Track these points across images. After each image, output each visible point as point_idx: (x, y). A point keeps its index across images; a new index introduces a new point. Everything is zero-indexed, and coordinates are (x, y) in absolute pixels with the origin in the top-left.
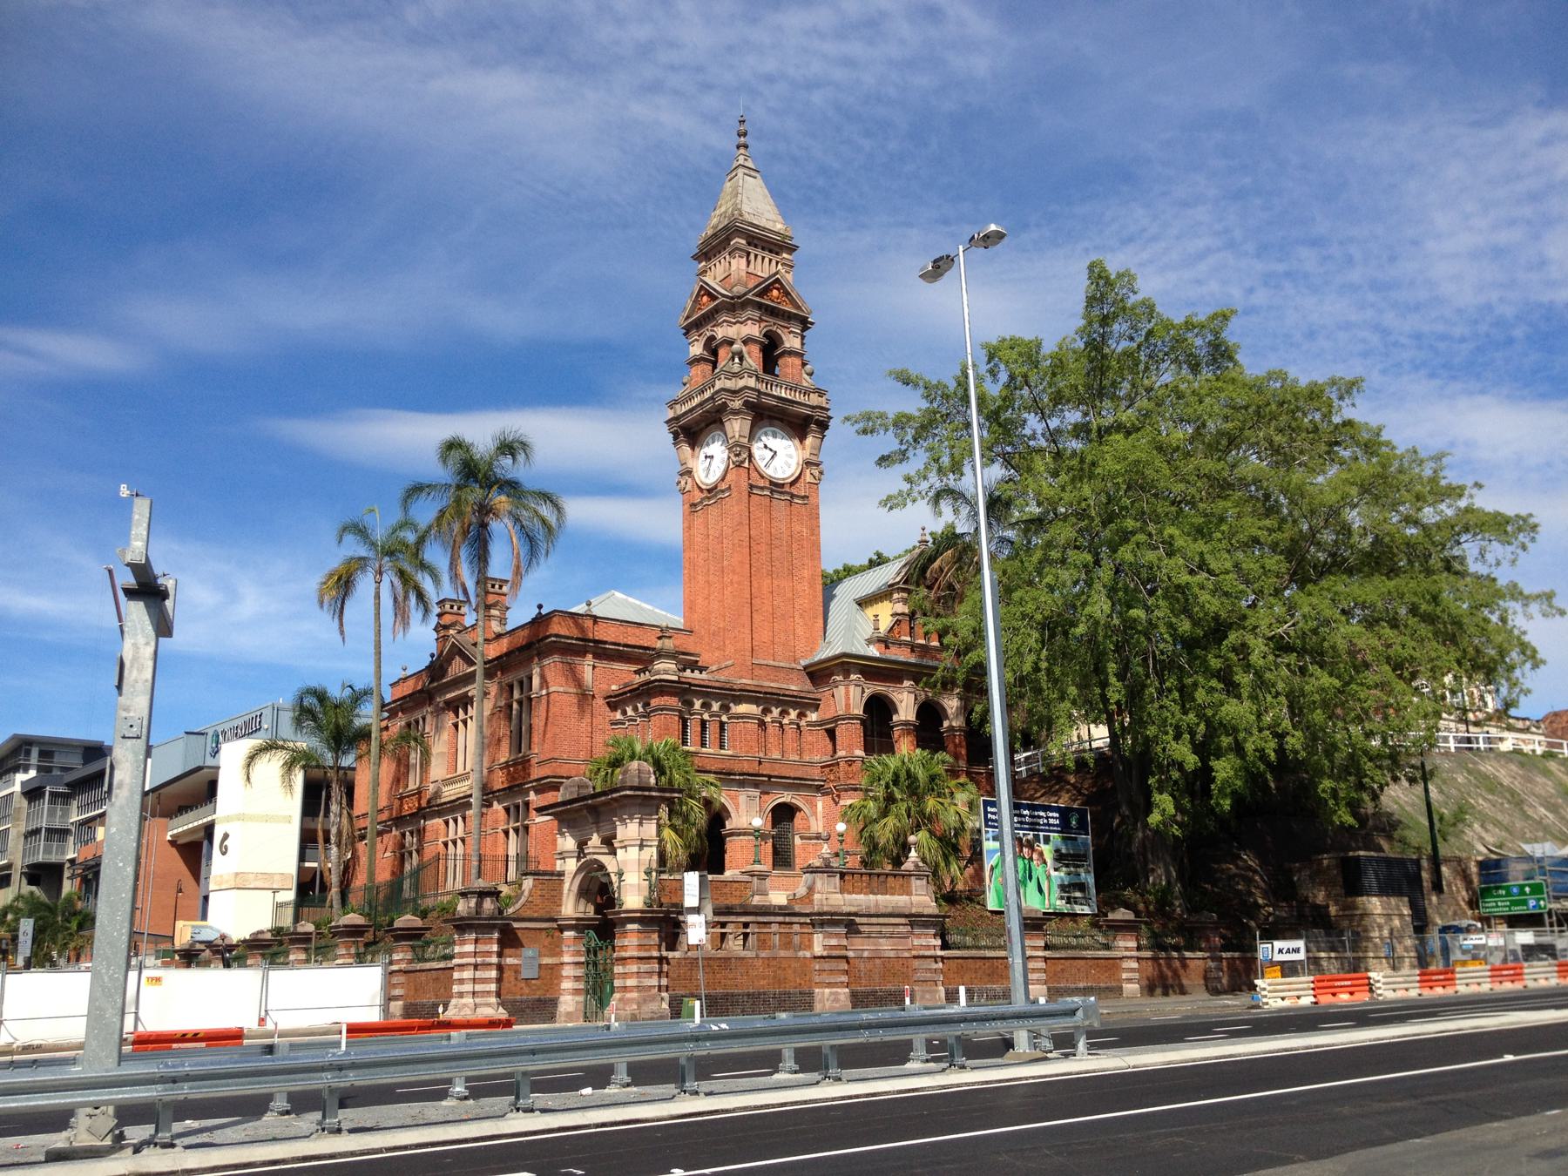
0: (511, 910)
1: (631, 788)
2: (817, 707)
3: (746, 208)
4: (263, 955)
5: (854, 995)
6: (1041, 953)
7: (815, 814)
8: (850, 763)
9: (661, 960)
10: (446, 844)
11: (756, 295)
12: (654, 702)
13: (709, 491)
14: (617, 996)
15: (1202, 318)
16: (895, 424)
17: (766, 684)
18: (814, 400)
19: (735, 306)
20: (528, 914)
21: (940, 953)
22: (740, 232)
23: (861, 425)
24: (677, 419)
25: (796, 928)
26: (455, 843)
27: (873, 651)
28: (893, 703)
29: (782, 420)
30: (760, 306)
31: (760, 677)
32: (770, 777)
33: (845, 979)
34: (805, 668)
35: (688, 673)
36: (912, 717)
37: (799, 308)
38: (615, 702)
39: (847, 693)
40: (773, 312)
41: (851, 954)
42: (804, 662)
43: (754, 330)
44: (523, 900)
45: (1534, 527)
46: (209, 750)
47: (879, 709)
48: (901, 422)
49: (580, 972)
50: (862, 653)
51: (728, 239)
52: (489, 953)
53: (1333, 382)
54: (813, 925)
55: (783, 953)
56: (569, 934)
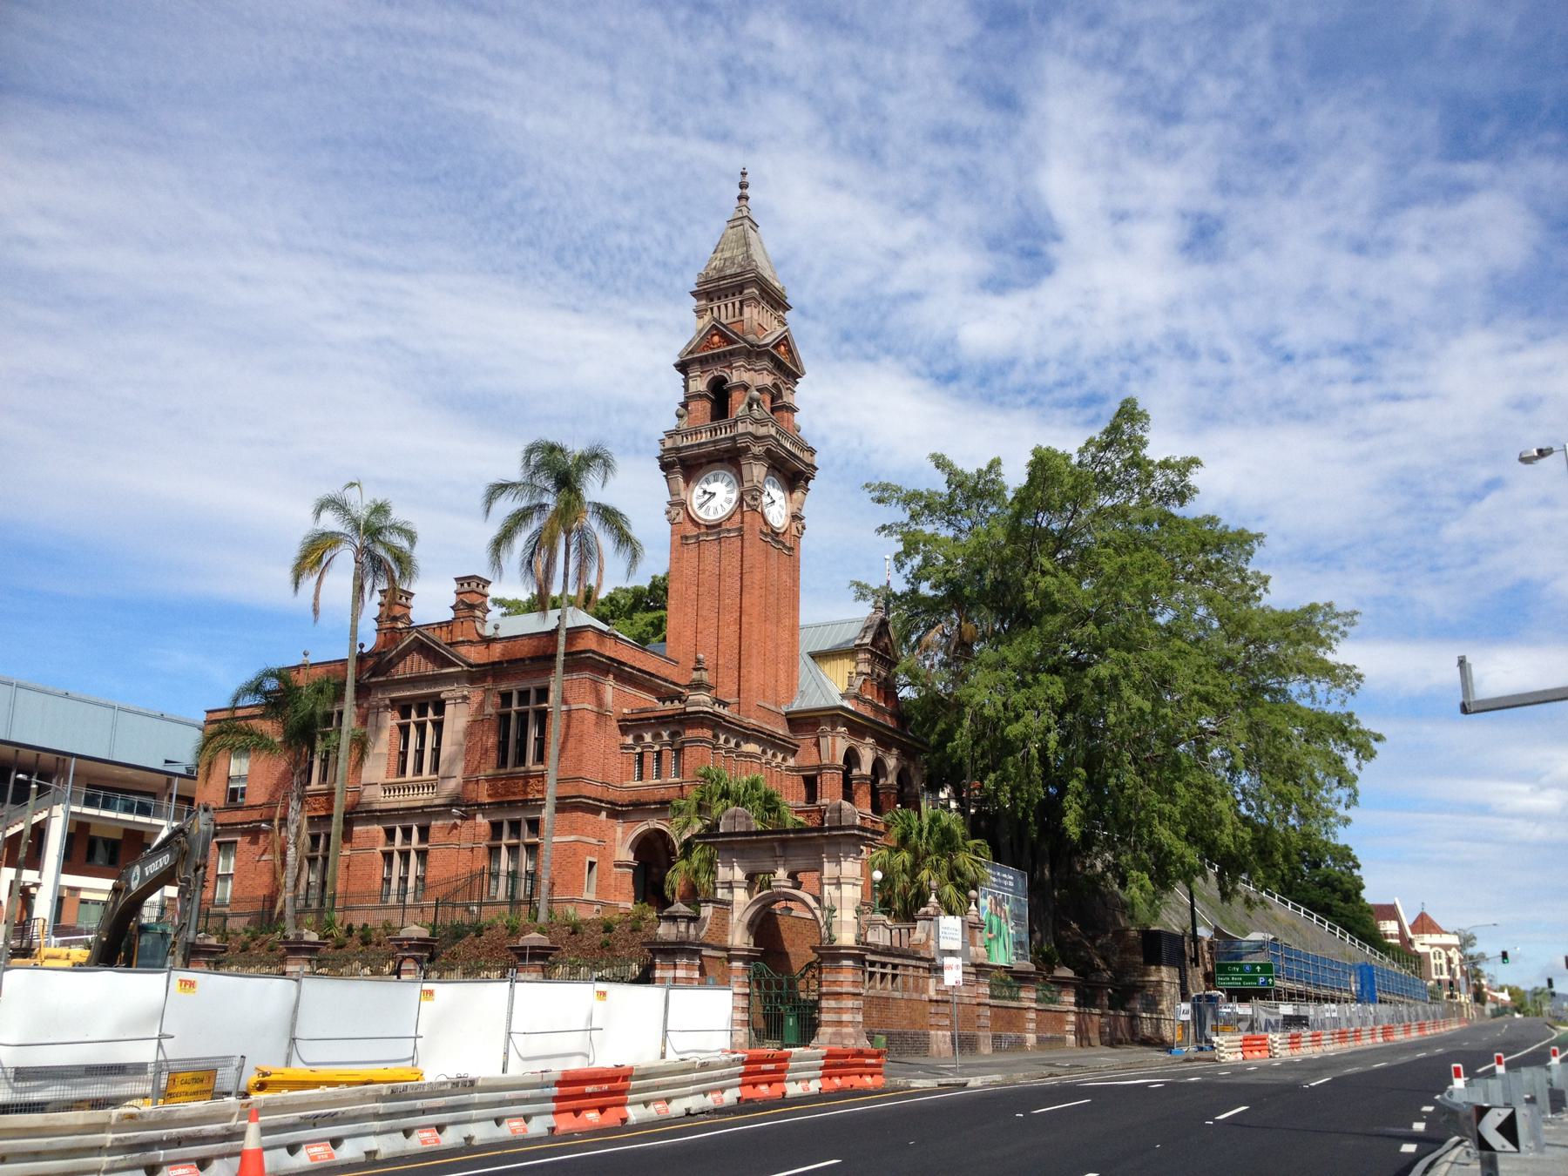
2: (794, 753)
4: (208, 963)
6: (1034, 1005)
10: (388, 856)
12: (690, 734)
19: (754, 353)
21: (988, 1001)
23: (877, 494)
26: (405, 855)
38: (629, 725)
39: (834, 744)
42: (784, 709)
43: (767, 380)
45: (1359, 677)
48: (911, 498)
51: (740, 288)
54: (929, 970)
56: (737, 965)
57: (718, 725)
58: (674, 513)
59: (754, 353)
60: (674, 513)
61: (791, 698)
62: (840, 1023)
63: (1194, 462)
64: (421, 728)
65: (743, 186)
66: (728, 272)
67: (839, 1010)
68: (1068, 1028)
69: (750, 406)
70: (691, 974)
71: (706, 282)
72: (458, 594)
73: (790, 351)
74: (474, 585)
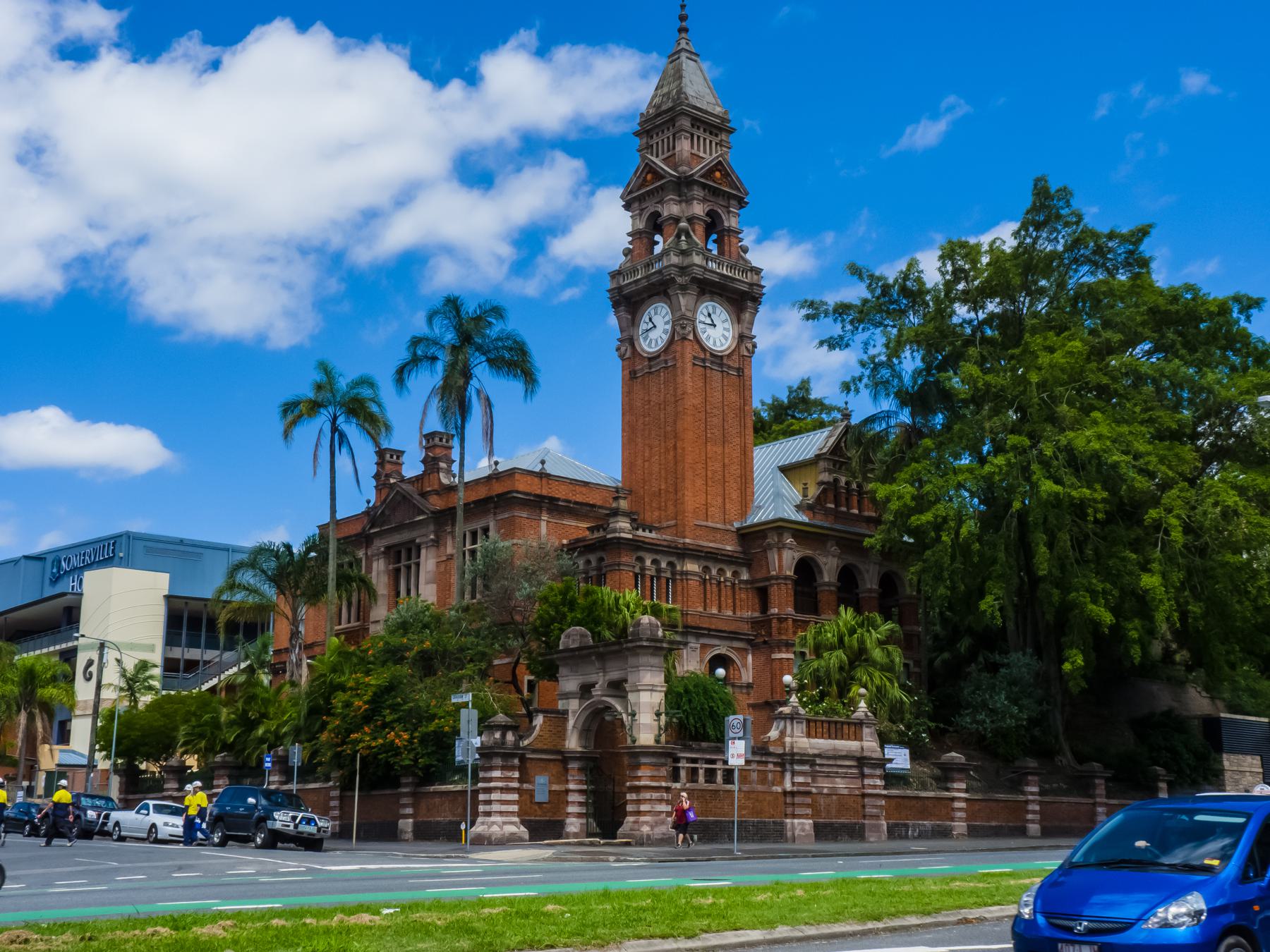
0: (526, 742)
1: (648, 640)
5: (816, 826)
6: (963, 795)
7: (745, 665)
8: (781, 620)
9: (668, 789)
11: (702, 176)
13: (650, 359)
14: (630, 819)
15: (1125, 230)
16: (835, 311)
17: (705, 544)
18: (750, 278)
19: (683, 185)
22: (684, 113)
24: (620, 289)
25: (771, 767)
27: (803, 518)
29: (721, 295)
30: (704, 186)
33: (809, 811)
34: (738, 529)
35: (640, 532)
36: (834, 579)
37: (738, 189)
40: (715, 192)
41: (814, 790)
42: (737, 525)
46: (48, 575)
48: (842, 310)
49: (581, 799)
50: (793, 518)
51: (672, 121)
53: (1237, 299)
55: (760, 788)
56: (573, 765)
58: (623, 349)
60: (623, 349)
61: (744, 514)
62: (639, 813)
65: (683, 18)
66: (664, 108)
67: (638, 802)
68: (1030, 816)
69: (678, 236)
70: (510, 774)
72: (427, 449)
73: (726, 175)
74: (437, 440)
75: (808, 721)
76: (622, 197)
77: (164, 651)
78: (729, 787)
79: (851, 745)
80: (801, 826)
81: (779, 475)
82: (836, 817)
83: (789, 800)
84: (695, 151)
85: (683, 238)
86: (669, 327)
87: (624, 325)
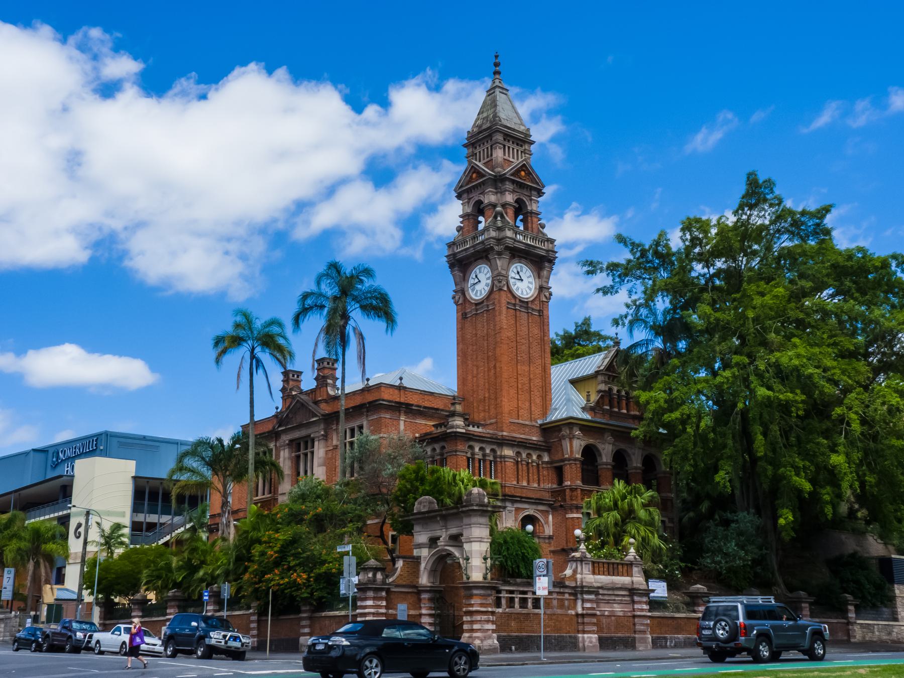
0: (391, 580)
1: (477, 505)
3: (502, 115)
5: (600, 639)
7: (547, 523)
8: (572, 490)
11: (512, 175)
13: (476, 304)
18: (546, 246)
19: (498, 181)
20: (401, 582)
21: (649, 614)
22: (498, 131)
24: (454, 255)
25: (567, 596)
27: (587, 416)
28: (598, 451)
30: (513, 182)
31: (514, 431)
32: (521, 497)
33: (595, 628)
34: (541, 425)
35: (471, 428)
36: (610, 460)
40: (521, 186)
41: (598, 613)
42: (540, 422)
44: (396, 575)
46: (50, 463)
47: (590, 453)
48: (613, 267)
50: (580, 416)
51: (490, 136)
52: (380, 607)
55: (559, 611)
56: (425, 596)
57: (470, 439)
58: (457, 297)
59: (498, 181)
60: (457, 297)
63: (827, 210)
64: (306, 455)
65: (497, 65)
66: (484, 127)
69: (495, 217)
71: (471, 137)
73: (529, 174)
74: (325, 363)
75: (593, 563)
76: (455, 190)
77: (132, 516)
78: (537, 611)
79: (625, 580)
80: (590, 639)
81: (570, 386)
82: (615, 633)
83: (580, 620)
84: (506, 157)
85: (499, 218)
86: (489, 281)
87: (458, 280)
